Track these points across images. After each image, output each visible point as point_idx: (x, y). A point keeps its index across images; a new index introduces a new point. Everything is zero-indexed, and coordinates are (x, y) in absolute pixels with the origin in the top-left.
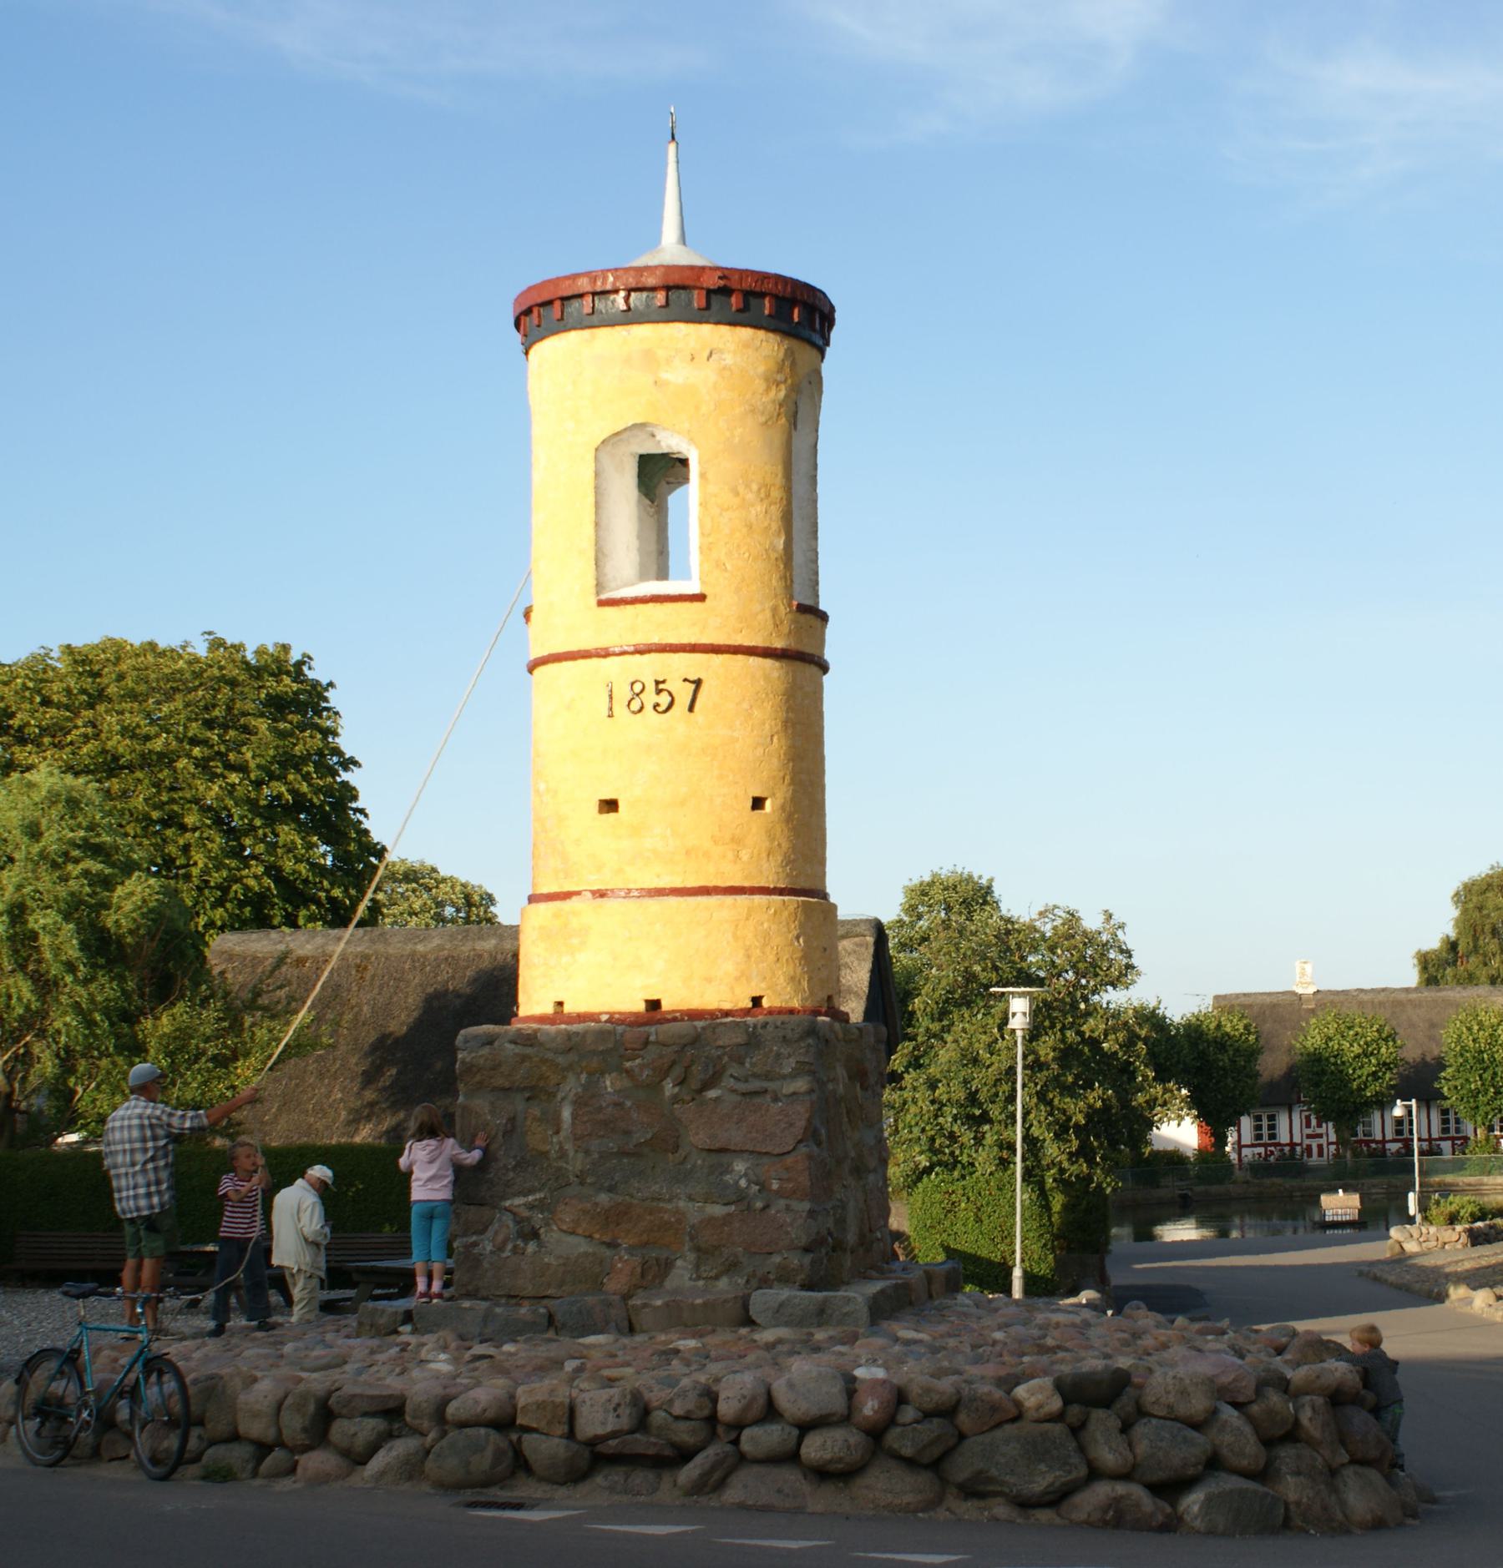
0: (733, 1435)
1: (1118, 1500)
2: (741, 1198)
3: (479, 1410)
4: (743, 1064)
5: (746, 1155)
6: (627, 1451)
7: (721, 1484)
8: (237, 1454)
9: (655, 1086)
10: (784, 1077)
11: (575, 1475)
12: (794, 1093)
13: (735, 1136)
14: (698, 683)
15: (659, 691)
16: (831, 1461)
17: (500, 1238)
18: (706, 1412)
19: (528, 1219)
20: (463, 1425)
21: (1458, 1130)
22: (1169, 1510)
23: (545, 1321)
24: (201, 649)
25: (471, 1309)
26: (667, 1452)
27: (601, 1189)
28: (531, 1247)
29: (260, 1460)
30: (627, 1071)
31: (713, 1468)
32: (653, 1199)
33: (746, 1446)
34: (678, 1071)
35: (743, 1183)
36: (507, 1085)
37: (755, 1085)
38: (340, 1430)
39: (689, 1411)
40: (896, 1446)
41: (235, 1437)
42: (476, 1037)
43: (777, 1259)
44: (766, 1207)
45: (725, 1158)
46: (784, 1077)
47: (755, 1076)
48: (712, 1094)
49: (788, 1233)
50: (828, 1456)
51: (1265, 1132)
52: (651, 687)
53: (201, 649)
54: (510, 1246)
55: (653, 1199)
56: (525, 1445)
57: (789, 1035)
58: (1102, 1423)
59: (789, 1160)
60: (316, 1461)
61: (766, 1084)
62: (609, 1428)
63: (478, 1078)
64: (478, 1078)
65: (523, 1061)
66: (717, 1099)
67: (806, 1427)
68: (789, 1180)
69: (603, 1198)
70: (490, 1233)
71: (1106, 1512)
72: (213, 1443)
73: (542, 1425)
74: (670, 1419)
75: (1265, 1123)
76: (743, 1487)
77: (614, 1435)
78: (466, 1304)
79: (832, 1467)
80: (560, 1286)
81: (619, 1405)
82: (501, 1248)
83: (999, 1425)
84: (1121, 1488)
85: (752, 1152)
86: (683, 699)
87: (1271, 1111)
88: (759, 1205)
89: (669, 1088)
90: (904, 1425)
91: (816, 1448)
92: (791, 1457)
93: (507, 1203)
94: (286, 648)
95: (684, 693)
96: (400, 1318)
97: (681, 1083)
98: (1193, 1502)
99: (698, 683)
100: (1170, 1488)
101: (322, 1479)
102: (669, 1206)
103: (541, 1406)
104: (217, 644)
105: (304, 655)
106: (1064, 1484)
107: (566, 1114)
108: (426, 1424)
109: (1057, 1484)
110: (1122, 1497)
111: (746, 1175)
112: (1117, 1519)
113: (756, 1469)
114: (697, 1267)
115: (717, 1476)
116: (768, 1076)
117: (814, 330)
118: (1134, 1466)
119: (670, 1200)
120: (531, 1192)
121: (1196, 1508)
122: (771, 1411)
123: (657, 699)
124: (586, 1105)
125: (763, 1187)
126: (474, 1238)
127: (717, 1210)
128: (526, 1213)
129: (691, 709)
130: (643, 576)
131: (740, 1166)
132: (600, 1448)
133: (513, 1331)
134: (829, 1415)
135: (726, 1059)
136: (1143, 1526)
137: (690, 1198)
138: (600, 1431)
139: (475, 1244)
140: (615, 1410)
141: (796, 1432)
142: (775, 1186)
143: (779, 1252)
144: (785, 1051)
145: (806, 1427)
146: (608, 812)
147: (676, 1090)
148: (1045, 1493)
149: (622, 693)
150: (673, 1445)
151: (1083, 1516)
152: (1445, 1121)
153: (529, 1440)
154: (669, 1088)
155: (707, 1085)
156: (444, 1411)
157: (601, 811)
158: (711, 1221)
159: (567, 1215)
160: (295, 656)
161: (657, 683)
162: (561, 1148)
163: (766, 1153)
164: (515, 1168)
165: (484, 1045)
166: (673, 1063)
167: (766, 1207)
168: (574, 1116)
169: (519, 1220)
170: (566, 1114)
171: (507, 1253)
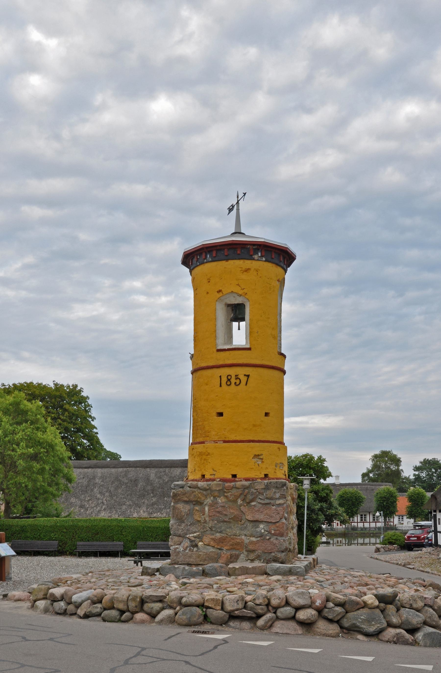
0: (274, 611)
1: (397, 634)
2: (261, 535)
3: (194, 601)
4: (263, 495)
5: (263, 523)
6: (241, 615)
7: (271, 626)
8: (114, 613)
9: (235, 501)
10: (276, 499)
11: (223, 623)
12: (280, 504)
13: (260, 517)
14: (248, 376)
15: (236, 379)
16: (306, 620)
17: (185, 546)
18: (266, 603)
19: (194, 541)
20: (186, 605)
21: (365, 520)
22: (413, 638)
23: (202, 572)
24: (52, 385)
25: (178, 568)
26: (254, 615)
27: (217, 532)
28: (195, 549)
29: (121, 615)
30: (226, 496)
31: (269, 620)
32: (234, 535)
33: (279, 614)
34: (242, 497)
35: (263, 531)
36: (188, 500)
37: (267, 501)
38: (146, 607)
39: (261, 603)
40: (326, 615)
41: (113, 608)
42: (178, 485)
43: (273, 554)
44: (270, 538)
45: (257, 524)
46: (276, 499)
47: (267, 498)
48: (253, 504)
49: (277, 546)
50: (305, 618)
51: (363, 519)
52: (233, 377)
53: (52, 385)
54: (188, 549)
55: (234, 535)
56: (208, 613)
57: (278, 486)
58: (391, 608)
59: (278, 524)
60: (140, 616)
61: (271, 501)
62: (235, 608)
63: (179, 497)
64: (179, 497)
65: (193, 493)
66: (254, 505)
67: (297, 609)
68: (277, 530)
69: (218, 535)
70: (182, 544)
71: (394, 638)
72: (105, 609)
73: (213, 606)
74: (255, 605)
75: (363, 517)
76: (279, 627)
77: (237, 610)
78: (176, 566)
79: (306, 622)
80: (204, 561)
81: (238, 600)
82: (185, 549)
83: (358, 609)
84: (398, 631)
85: (265, 522)
86: (243, 382)
87: (365, 513)
88: (268, 538)
89: (240, 502)
90: (329, 608)
91: (302, 615)
92: (293, 618)
93: (188, 536)
94: (76, 386)
95: (244, 379)
96: (156, 570)
97: (243, 500)
98: (419, 635)
99: (248, 376)
100: (412, 631)
101: (142, 622)
102: (239, 537)
103: (213, 600)
104: (56, 385)
105: (81, 388)
106: (380, 629)
107: (207, 509)
108: (175, 605)
109: (378, 629)
110: (398, 633)
111: (263, 528)
112: (398, 640)
113: (282, 622)
114: (247, 556)
115: (270, 623)
116: (271, 499)
117: (285, 264)
118: (402, 623)
119: (239, 536)
120: (195, 532)
121: (420, 638)
122: (287, 603)
123: (236, 381)
124: (213, 506)
125: (269, 532)
126: (176, 546)
127: (254, 539)
128: (193, 539)
129: (246, 385)
130: (225, 344)
131: (262, 526)
132: (232, 614)
133: (193, 575)
134: (306, 605)
135: (258, 493)
136: (406, 643)
137: (246, 535)
138: (232, 609)
139: (178, 548)
140: (237, 602)
141: (294, 610)
142: (273, 532)
143: (274, 552)
144: (277, 491)
145: (297, 609)
146: (220, 416)
147: (242, 502)
148: (374, 632)
149: (224, 379)
150: (256, 613)
151: (387, 639)
152: (374, 518)
153: (209, 611)
154: (240, 502)
155: (252, 501)
156: (181, 601)
157: (217, 416)
158: (252, 543)
159: (206, 539)
160: (79, 388)
161: (236, 376)
162: (205, 519)
163: (271, 522)
164: (190, 525)
165: (181, 488)
166: (241, 494)
167: (270, 538)
168: (209, 510)
169: (191, 541)
170: (207, 509)
171: (187, 551)
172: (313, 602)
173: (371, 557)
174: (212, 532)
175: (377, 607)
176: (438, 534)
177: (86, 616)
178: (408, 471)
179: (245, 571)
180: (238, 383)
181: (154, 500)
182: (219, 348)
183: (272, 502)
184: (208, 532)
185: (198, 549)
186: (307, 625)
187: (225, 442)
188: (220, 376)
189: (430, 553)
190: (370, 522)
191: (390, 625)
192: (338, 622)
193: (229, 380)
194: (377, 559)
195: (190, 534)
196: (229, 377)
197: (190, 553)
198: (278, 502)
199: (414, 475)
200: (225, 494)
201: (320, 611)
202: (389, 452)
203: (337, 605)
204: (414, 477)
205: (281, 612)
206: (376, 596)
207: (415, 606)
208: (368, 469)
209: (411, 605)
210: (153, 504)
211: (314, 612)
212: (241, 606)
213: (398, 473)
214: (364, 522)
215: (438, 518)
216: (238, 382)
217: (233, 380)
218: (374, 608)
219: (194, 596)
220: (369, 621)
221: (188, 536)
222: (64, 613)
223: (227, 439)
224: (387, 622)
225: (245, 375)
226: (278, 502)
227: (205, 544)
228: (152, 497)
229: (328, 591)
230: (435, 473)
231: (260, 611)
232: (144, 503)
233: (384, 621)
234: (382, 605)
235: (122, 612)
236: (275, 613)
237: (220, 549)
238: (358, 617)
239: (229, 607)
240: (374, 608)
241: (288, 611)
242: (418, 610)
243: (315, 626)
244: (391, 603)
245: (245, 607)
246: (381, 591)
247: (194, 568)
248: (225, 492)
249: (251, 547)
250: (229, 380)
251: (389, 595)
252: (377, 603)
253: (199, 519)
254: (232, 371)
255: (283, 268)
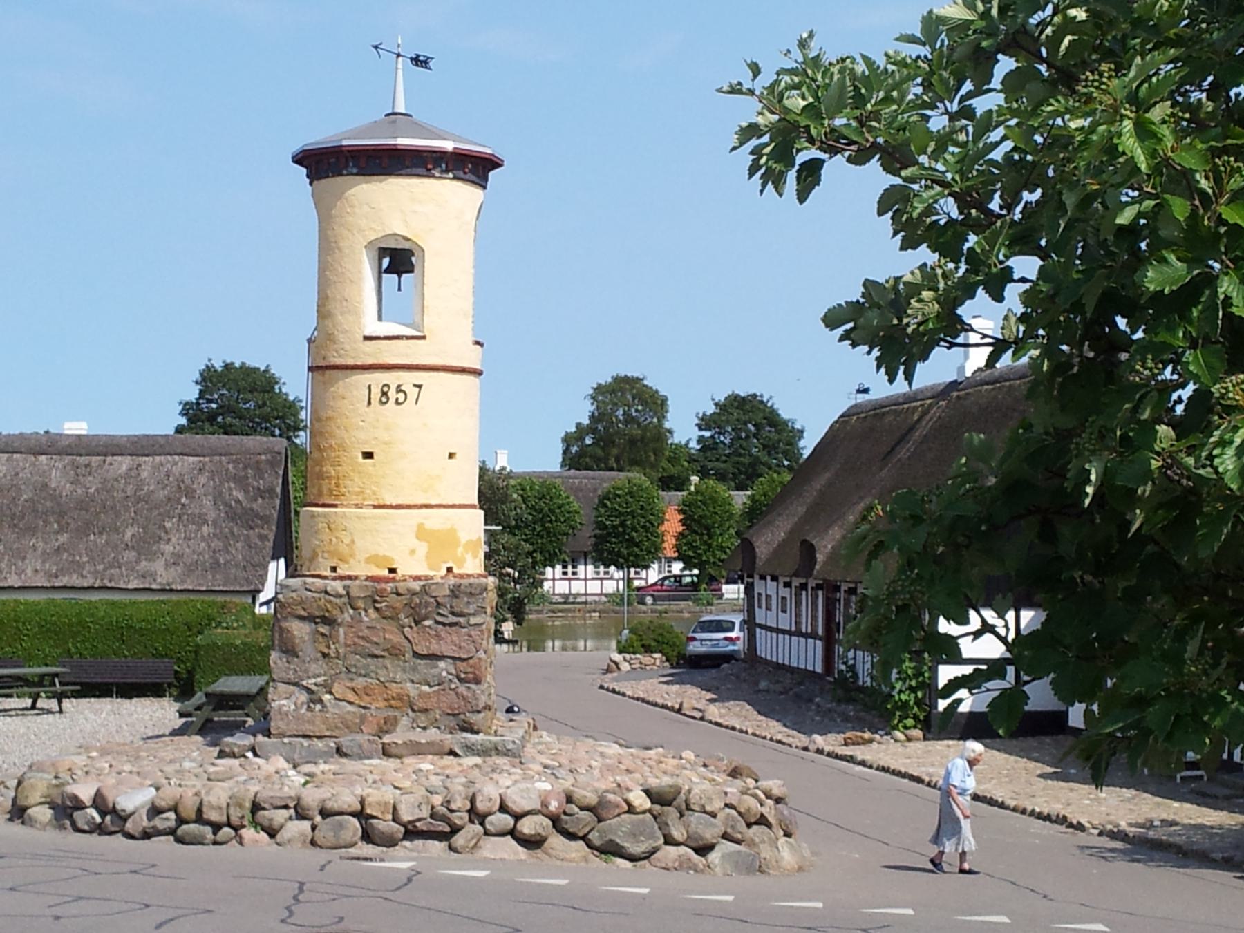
14: (420, 387)
17: (299, 702)
21: (574, 573)
26: (447, 829)
28: (318, 707)
47: (453, 613)
58: (671, 812)
70: (293, 699)
77: (419, 820)
83: (618, 815)
91: (528, 827)
98: (714, 856)
100: (704, 850)
112: (683, 865)
122: (503, 808)
131: (442, 664)
137: (413, 682)
138: (410, 818)
158: (422, 695)
168: (345, 634)
172: (545, 804)
173: (601, 687)
174: (350, 676)
175: (650, 811)
176: (758, 630)
177: (146, 835)
178: (683, 429)
179: (418, 750)
180: (401, 400)
181: (63, 538)
182: (367, 334)
183: (462, 620)
184: (343, 675)
185: (324, 706)
186: (532, 843)
187: (375, 507)
188: (369, 387)
189: (738, 677)
190: (586, 580)
191: (669, 841)
192: (584, 838)
193: (384, 394)
194: (613, 691)
195: (309, 677)
196: (385, 389)
197: (309, 714)
198: (473, 620)
199: (701, 440)
200: (378, 605)
201: (555, 820)
202: (638, 380)
203: (582, 809)
204: (699, 447)
205: (492, 824)
206: (647, 792)
207: (708, 808)
208: (578, 425)
209: (703, 806)
210: (58, 550)
211: (547, 822)
212: (425, 813)
213: (661, 435)
214: (570, 580)
215: (756, 591)
216: (401, 396)
217: (392, 394)
218: (644, 812)
219: (347, 799)
220: (634, 835)
221: (304, 683)
222: (100, 829)
223: (381, 503)
224: (664, 836)
225: (415, 386)
226: (473, 620)
227: (336, 699)
228: (57, 533)
229: (567, 783)
230: (755, 436)
231: (458, 822)
232: (34, 548)
233: (659, 834)
234: (657, 807)
235: (217, 827)
236: (482, 824)
237: (364, 708)
238: (618, 828)
239: (406, 817)
240: (644, 812)
241: (502, 821)
242: (714, 815)
243: (546, 845)
244: (670, 805)
245: (433, 816)
246: (653, 782)
247: (320, 745)
248: (375, 601)
249: (420, 704)
250: (384, 394)
251: (667, 789)
252: (648, 804)
253: (326, 651)
254: (392, 378)
255: (481, 185)
